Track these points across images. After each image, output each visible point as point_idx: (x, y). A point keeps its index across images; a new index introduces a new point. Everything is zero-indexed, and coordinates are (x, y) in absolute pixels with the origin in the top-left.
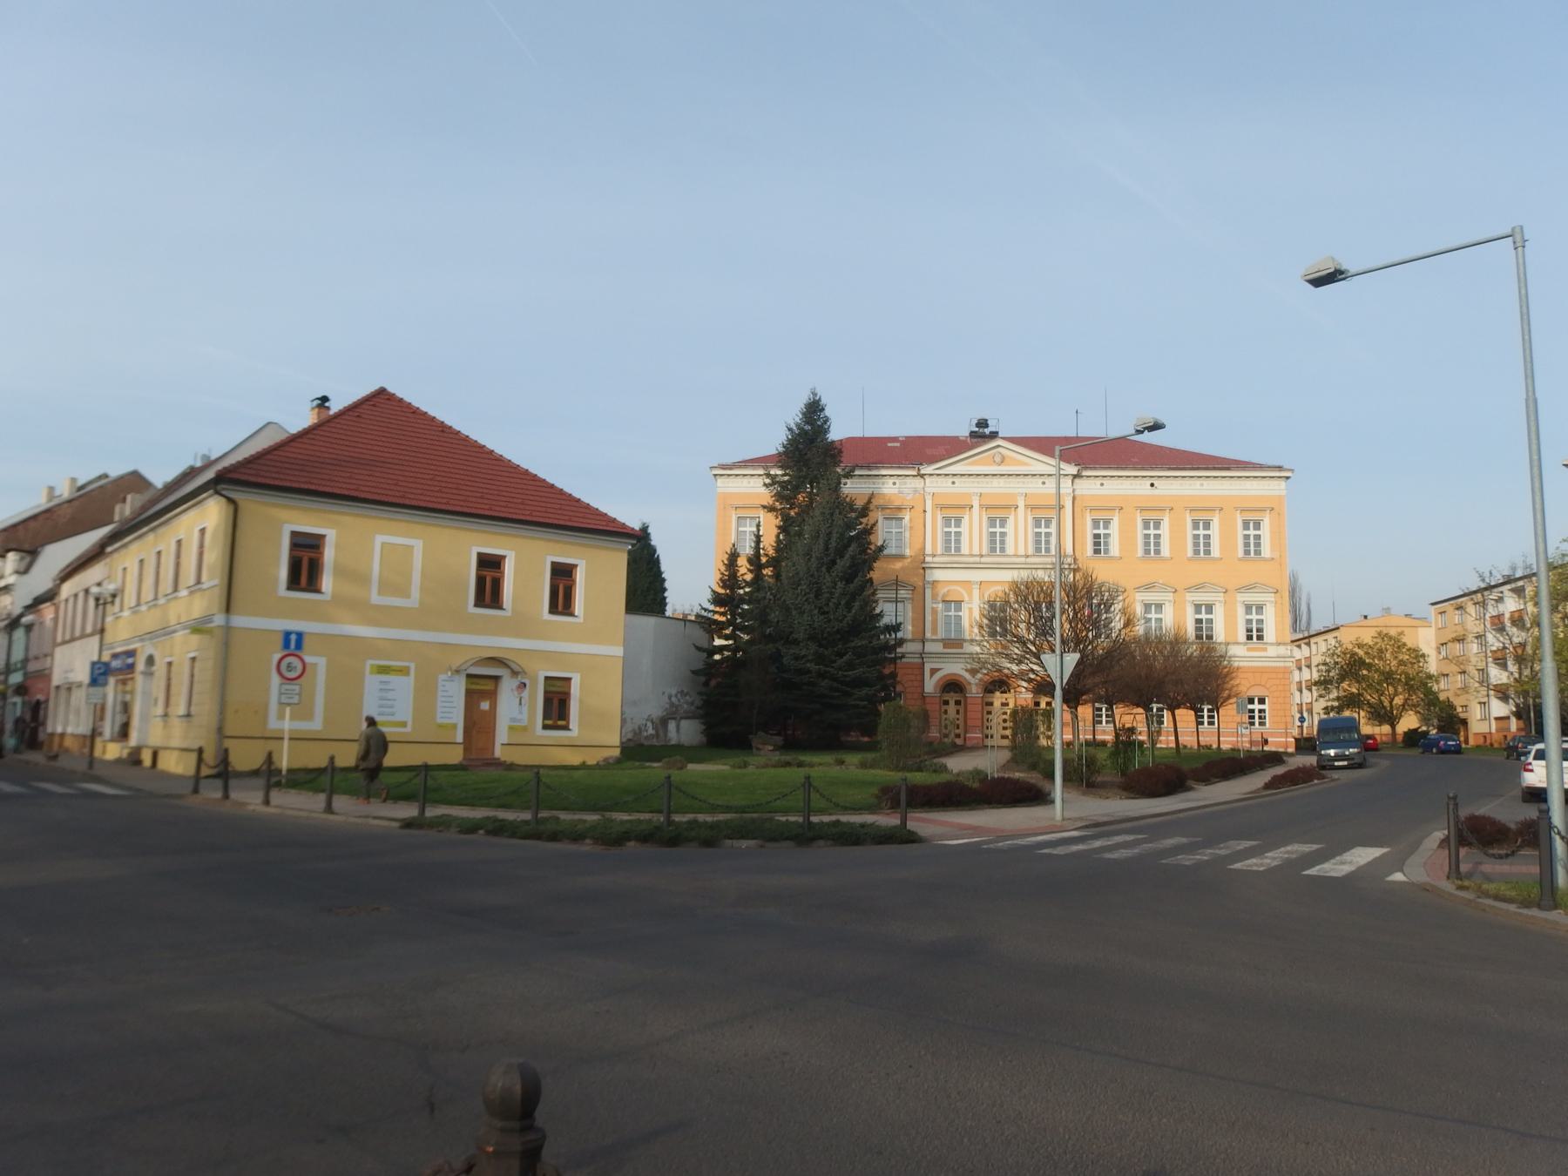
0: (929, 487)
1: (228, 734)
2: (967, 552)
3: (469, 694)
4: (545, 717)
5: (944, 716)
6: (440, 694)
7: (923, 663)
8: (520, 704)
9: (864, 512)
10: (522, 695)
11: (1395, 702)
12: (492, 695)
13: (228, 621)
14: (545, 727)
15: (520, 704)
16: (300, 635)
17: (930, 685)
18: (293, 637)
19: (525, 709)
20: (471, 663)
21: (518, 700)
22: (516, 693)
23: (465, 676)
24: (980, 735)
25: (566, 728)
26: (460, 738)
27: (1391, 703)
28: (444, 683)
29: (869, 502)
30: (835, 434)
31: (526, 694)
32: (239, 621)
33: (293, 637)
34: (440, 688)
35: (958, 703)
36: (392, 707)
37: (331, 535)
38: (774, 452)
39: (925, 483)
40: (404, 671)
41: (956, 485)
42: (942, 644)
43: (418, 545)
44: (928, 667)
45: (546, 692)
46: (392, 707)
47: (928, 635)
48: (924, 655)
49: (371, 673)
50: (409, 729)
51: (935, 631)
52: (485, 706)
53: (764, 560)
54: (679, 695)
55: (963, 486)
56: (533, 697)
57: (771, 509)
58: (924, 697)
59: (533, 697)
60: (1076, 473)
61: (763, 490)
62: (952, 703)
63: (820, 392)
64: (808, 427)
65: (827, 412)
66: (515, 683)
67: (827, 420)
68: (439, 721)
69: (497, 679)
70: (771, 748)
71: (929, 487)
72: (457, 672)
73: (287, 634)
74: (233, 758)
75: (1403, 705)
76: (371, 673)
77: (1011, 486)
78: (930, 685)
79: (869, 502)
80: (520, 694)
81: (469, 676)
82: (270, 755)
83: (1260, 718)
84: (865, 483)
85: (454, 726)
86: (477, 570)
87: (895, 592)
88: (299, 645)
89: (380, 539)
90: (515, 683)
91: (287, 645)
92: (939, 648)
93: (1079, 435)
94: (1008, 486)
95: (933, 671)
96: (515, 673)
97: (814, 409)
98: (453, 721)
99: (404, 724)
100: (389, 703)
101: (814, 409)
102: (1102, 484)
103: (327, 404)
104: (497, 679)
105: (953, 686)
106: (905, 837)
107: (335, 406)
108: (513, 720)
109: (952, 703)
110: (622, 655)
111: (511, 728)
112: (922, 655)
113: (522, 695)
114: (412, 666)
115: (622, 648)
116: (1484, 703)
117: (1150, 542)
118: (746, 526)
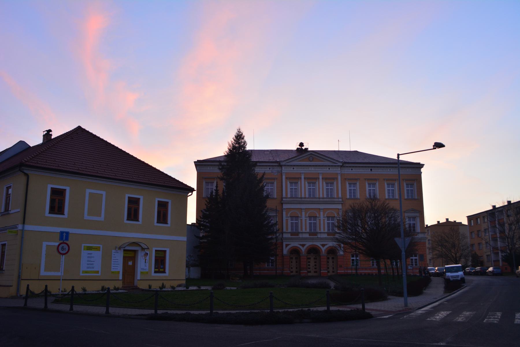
0: (283, 170)
1: (23, 278)
2: (318, 196)
3: (124, 258)
4: (155, 268)
5: (291, 264)
6: (113, 258)
7: (283, 242)
8: (145, 262)
9: (261, 180)
10: (146, 258)
11: (457, 256)
12: (134, 258)
13: (23, 227)
14: (155, 272)
15: (145, 262)
16: (67, 233)
17: (285, 251)
18: (65, 234)
19: (147, 264)
20: (127, 244)
21: (145, 260)
22: (143, 257)
23: (123, 250)
24: (306, 271)
25: (164, 272)
26: (121, 278)
27: (456, 255)
28: (114, 254)
29: (263, 176)
30: (249, 148)
31: (148, 258)
32: (28, 227)
33: (65, 234)
34: (113, 256)
35: (333, 258)
36: (92, 264)
37: (68, 189)
38: (223, 155)
39: (282, 169)
40: (98, 249)
41: (295, 169)
42: (308, 234)
43: (104, 193)
44: (284, 244)
45: (156, 257)
46: (92, 264)
47: (284, 230)
48: (283, 239)
49: (84, 250)
50: (99, 274)
51: (287, 229)
52: (130, 263)
53: (219, 200)
54: (189, 257)
55: (296, 170)
56: (150, 259)
57: (222, 179)
58: (283, 256)
59: (150, 259)
60: (342, 165)
61: (218, 171)
62: (330, 258)
63: (242, 130)
64: (237, 145)
65: (246, 139)
66: (143, 253)
67: (245, 142)
68: (112, 270)
69: (135, 252)
70: (238, 279)
71: (283, 170)
72: (120, 248)
73: (62, 233)
74: (75, 289)
75: (460, 256)
76: (84, 250)
77: (317, 170)
78: (285, 251)
79: (263, 176)
80: (146, 257)
81: (124, 250)
82: (73, 287)
83: (415, 262)
84: (325, 169)
85: (119, 272)
86: (128, 204)
87: (275, 213)
88: (67, 239)
89: (88, 191)
90: (143, 253)
91: (61, 238)
92: (289, 236)
93: (339, 150)
94: (315, 170)
95: (287, 245)
96: (143, 249)
97: (239, 137)
98: (118, 270)
99: (98, 272)
100: (92, 262)
101: (239, 137)
102: (329, 169)
103: (50, 133)
104: (135, 252)
105: (295, 251)
106: (365, 316)
107: (55, 135)
108: (142, 269)
109: (330, 258)
110: (186, 240)
111: (141, 273)
112: (282, 239)
113: (146, 258)
114: (101, 246)
115: (186, 237)
116: (489, 255)
117: (390, 193)
118: (209, 186)
